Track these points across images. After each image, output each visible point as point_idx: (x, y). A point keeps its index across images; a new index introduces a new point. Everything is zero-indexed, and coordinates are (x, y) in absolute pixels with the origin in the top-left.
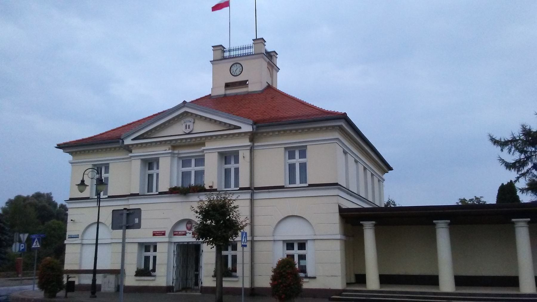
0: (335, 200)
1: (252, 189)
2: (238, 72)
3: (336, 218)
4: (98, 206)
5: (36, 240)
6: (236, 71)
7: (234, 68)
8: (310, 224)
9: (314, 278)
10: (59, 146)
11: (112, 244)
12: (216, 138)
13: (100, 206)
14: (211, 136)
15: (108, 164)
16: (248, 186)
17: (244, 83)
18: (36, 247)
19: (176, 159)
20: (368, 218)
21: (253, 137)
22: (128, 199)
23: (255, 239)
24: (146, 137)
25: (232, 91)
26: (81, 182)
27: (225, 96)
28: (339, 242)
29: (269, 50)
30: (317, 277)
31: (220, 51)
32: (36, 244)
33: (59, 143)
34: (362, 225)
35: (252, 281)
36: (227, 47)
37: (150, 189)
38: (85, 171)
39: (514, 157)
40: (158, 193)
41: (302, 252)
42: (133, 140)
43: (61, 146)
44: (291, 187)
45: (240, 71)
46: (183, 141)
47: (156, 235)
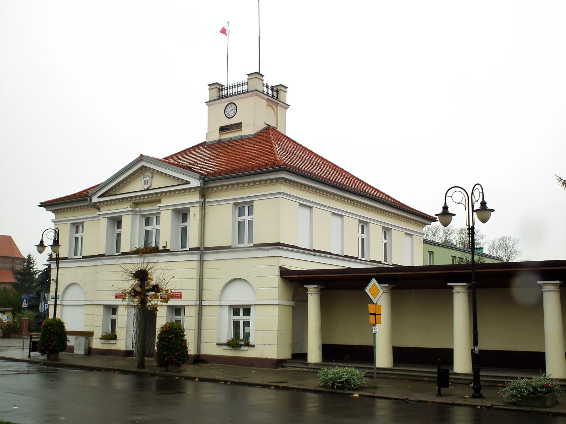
0: (275, 261)
2: (232, 113)
3: (276, 280)
4: (57, 267)
5: (25, 300)
6: (232, 110)
7: (229, 109)
8: (253, 288)
9: (254, 346)
10: (43, 205)
11: (85, 306)
12: (195, 190)
13: (59, 267)
15: (252, 202)
16: (196, 246)
17: (239, 126)
18: (25, 306)
19: (138, 217)
20: (311, 281)
21: (204, 192)
22: (96, 260)
24: (112, 194)
25: (227, 136)
26: (481, 205)
27: (220, 142)
28: (276, 309)
29: (272, 84)
30: (255, 345)
31: (216, 90)
32: (25, 304)
34: (307, 290)
35: (199, 348)
37: (183, 245)
38: (44, 232)
40: (120, 254)
42: (100, 197)
43: (43, 204)
44: (242, 247)
45: (234, 112)
46: (150, 197)
47: (118, 298)
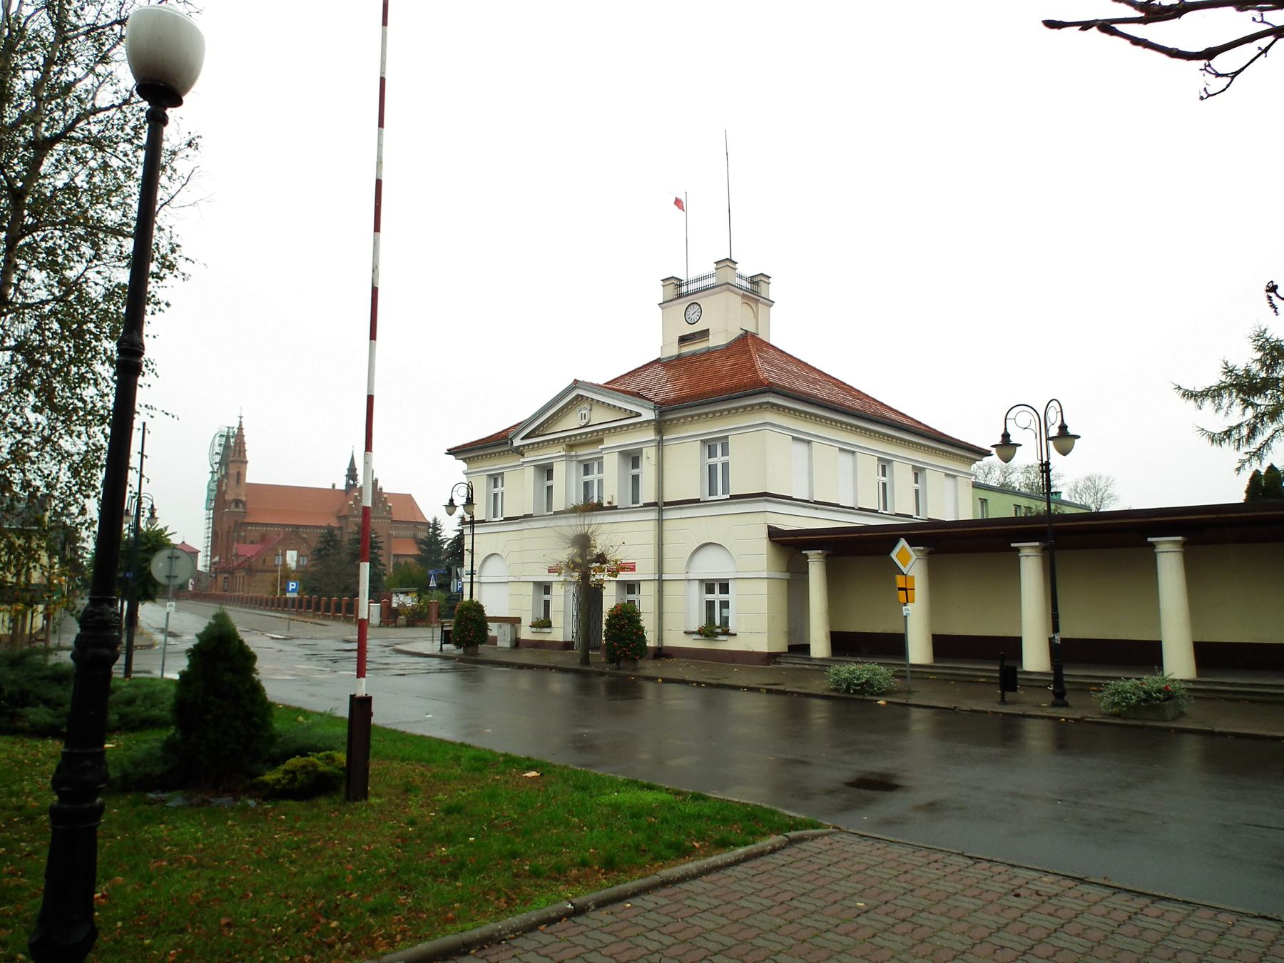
0: (761, 518)
1: (660, 506)
2: (695, 317)
5: (433, 577)
7: (691, 311)
10: (451, 452)
14: (609, 429)
17: (704, 334)
21: (660, 426)
22: (521, 522)
23: (665, 577)
27: (679, 357)
28: (764, 584)
33: (449, 448)
34: (806, 557)
35: (660, 639)
36: (683, 277)
39: (1236, 413)
41: (724, 597)
